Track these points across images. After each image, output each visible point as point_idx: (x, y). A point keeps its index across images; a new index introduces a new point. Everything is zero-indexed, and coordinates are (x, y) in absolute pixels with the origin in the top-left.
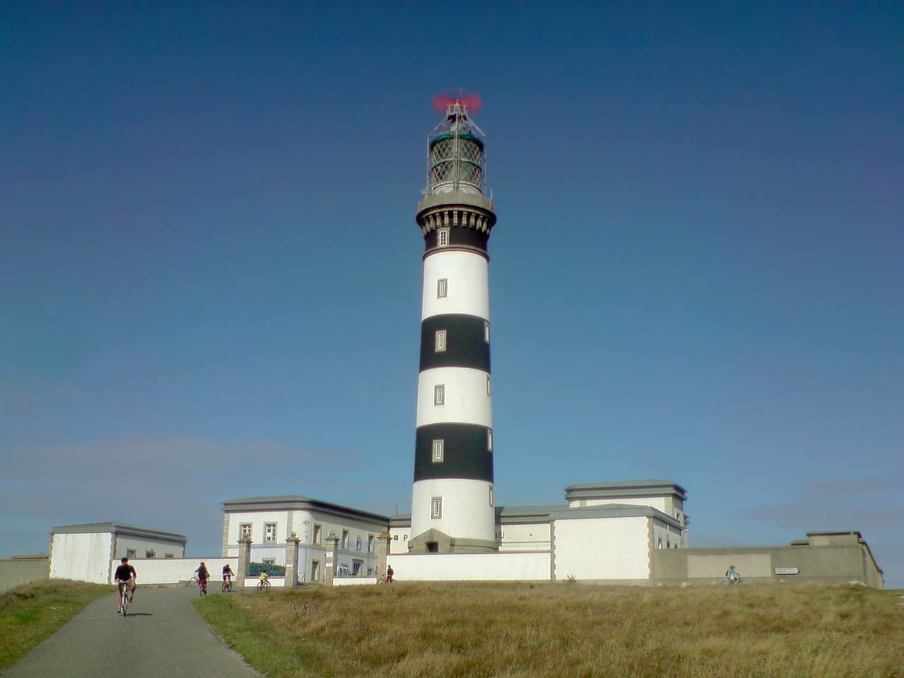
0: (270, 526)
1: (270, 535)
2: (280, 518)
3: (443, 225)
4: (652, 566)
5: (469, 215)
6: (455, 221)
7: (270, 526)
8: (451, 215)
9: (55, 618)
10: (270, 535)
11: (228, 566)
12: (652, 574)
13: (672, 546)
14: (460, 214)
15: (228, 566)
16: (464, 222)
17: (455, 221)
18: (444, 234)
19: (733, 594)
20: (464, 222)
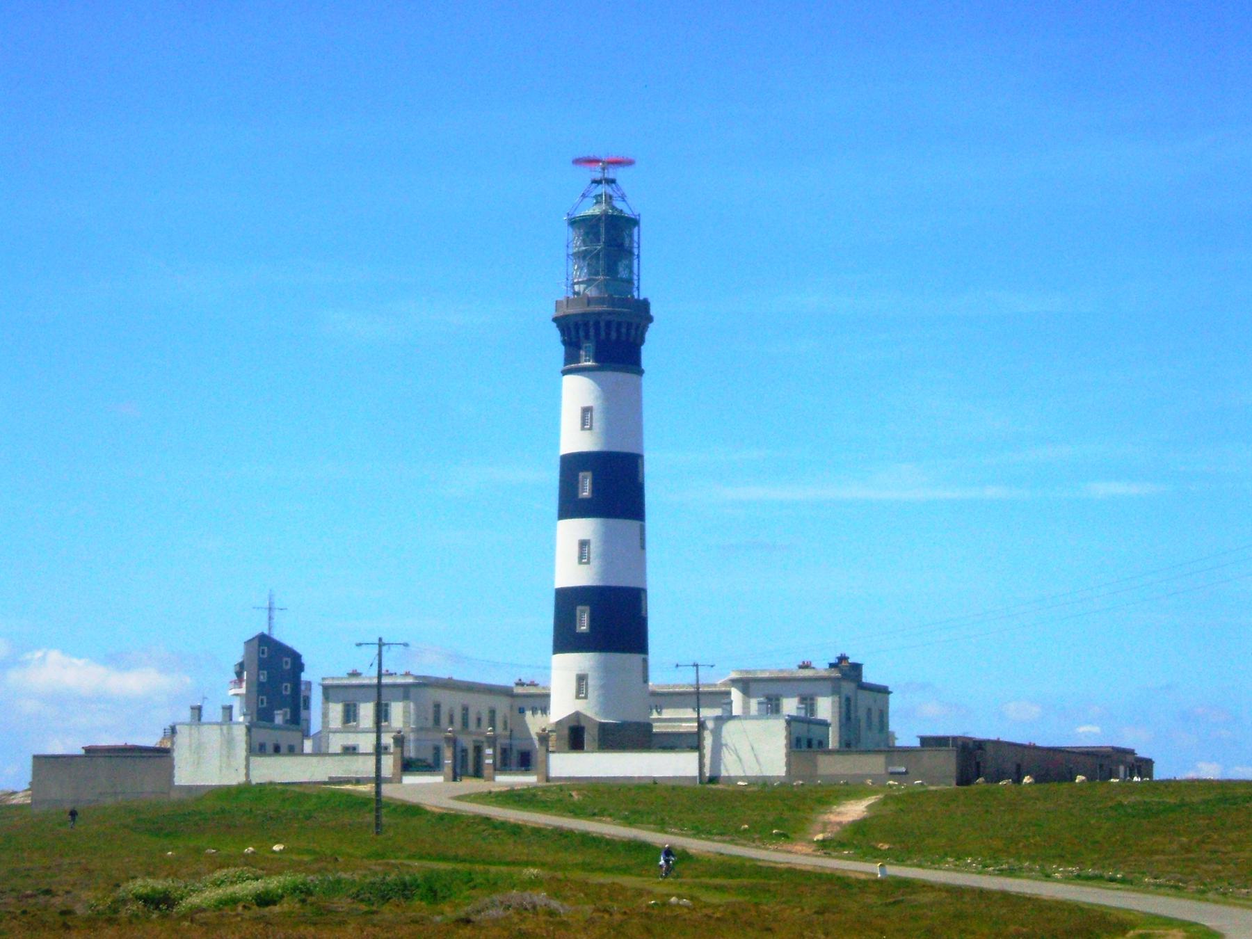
3: (587, 337)
12: (788, 771)
16: (614, 335)
20: (614, 335)
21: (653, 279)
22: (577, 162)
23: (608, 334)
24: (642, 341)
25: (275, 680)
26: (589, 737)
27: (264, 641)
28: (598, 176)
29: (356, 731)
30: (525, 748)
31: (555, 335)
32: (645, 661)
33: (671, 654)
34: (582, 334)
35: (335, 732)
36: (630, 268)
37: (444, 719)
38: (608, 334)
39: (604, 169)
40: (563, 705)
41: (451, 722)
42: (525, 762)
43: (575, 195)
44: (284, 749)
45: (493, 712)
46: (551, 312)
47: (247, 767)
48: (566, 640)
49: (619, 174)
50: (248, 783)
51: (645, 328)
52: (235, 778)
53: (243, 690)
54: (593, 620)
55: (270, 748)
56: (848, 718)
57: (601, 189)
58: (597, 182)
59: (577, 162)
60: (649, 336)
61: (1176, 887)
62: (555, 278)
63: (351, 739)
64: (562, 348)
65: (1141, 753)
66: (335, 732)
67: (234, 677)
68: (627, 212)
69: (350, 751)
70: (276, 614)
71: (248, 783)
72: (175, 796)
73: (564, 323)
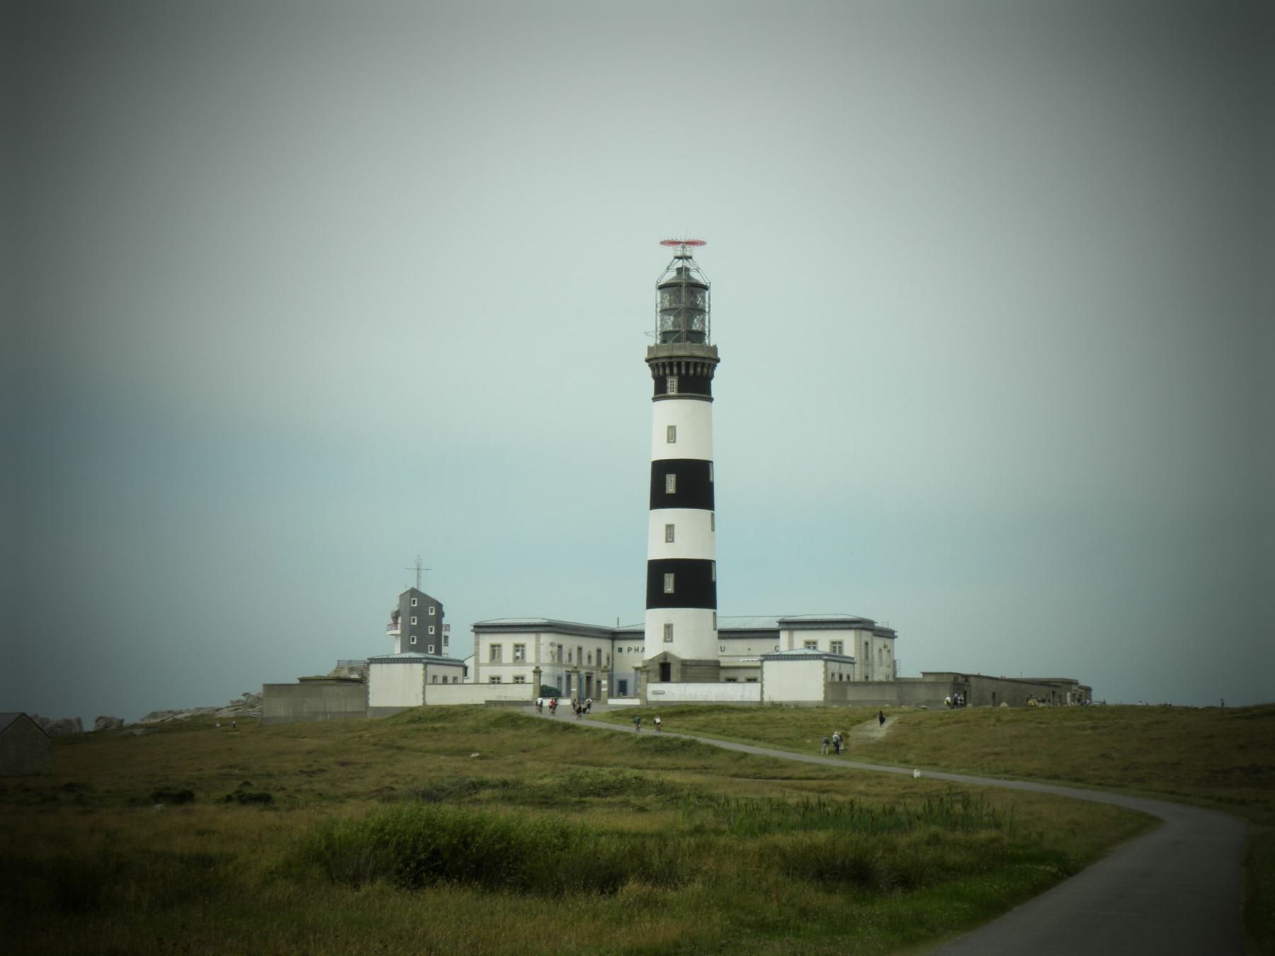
0: (518, 647)
1: (519, 654)
2: (528, 640)
3: (672, 374)
4: (825, 692)
5: (703, 365)
6: (683, 371)
7: (518, 647)
8: (679, 365)
9: (499, 908)
10: (519, 654)
11: (654, 399)
12: (825, 698)
13: (845, 679)
14: (688, 364)
15: (654, 399)
16: (691, 372)
17: (683, 371)
18: (672, 383)
19: (373, 881)
20: (691, 372)
21: (721, 328)
22: (663, 243)
23: (687, 370)
24: (712, 377)
25: (422, 624)
26: (674, 671)
27: (414, 592)
28: (679, 254)
29: (500, 664)
30: (623, 678)
31: (647, 372)
32: (715, 614)
33: (737, 601)
34: (668, 371)
35: (485, 665)
36: (703, 321)
37: (565, 657)
38: (687, 370)
39: (684, 247)
40: (653, 648)
41: (655, 693)
42: (622, 689)
43: (662, 267)
44: (450, 680)
45: (599, 651)
46: (645, 355)
47: (424, 693)
48: (656, 598)
49: (694, 251)
50: (762, 702)
51: (714, 366)
52: (414, 701)
53: (398, 632)
54: (679, 484)
55: (440, 680)
56: (867, 657)
57: (680, 264)
58: (679, 258)
59: (663, 243)
60: (717, 372)
61: (1100, 784)
62: (644, 325)
63: (496, 671)
64: (653, 382)
65: (1083, 683)
66: (485, 665)
67: (391, 622)
68: (702, 281)
69: (519, 680)
70: (423, 573)
71: (762, 702)
72: (370, 716)
73: (653, 362)
